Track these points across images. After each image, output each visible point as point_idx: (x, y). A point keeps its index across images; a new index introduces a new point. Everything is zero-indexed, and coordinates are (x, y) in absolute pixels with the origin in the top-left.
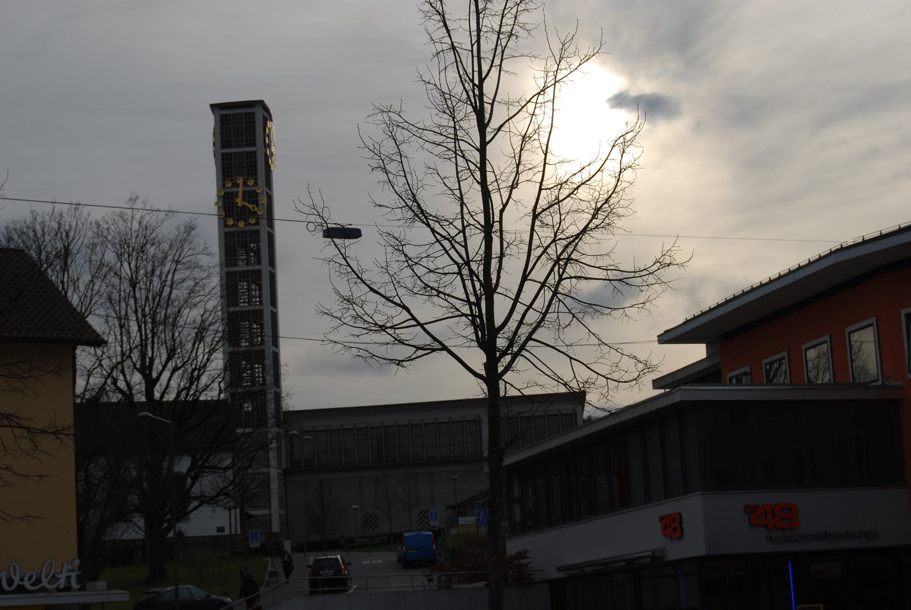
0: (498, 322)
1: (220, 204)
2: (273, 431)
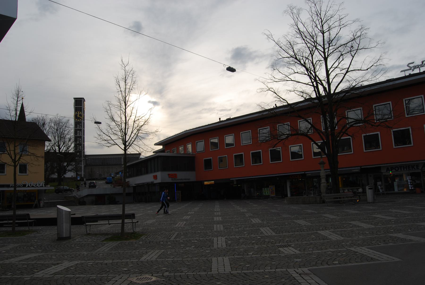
0: (127, 140)
2: (83, 158)
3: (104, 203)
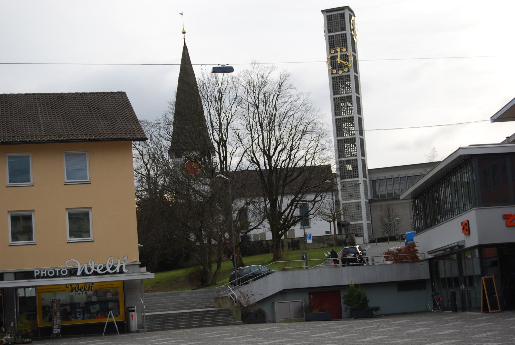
1: (329, 63)
3: (336, 316)
